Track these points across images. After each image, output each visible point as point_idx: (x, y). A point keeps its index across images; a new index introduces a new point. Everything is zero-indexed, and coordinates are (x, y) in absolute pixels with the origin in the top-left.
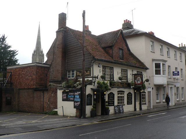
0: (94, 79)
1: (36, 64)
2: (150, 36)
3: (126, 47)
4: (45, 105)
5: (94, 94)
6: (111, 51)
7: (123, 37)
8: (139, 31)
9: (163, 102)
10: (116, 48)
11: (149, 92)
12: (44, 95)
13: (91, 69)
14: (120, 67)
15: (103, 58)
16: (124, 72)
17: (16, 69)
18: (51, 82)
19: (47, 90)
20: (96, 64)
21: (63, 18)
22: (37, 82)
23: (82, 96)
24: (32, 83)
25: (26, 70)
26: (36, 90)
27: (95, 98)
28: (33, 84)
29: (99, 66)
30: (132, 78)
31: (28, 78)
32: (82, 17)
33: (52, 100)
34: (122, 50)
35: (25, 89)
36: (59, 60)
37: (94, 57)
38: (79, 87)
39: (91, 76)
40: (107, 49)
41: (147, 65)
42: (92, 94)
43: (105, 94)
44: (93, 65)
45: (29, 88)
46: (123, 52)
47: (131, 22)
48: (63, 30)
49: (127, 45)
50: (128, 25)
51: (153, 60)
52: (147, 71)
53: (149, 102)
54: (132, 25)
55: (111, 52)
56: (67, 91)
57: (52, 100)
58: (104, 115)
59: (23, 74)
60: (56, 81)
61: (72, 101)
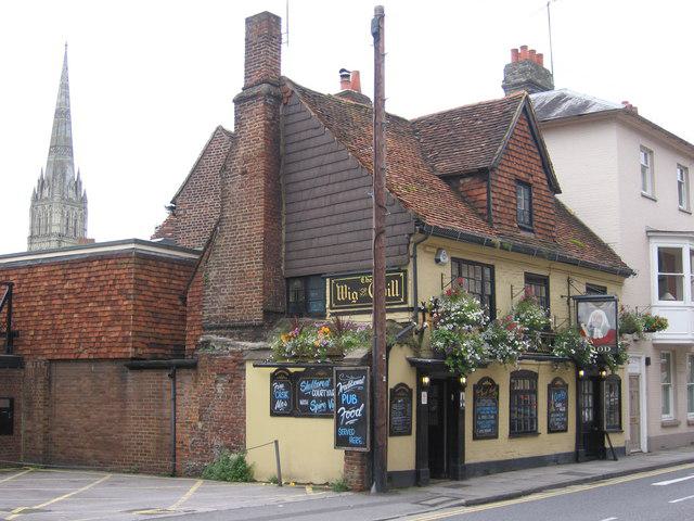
0: (420, 315)
1: (133, 246)
2: (627, 118)
3: (544, 177)
4: (184, 435)
5: (421, 386)
6: (485, 190)
7: (530, 125)
8: (586, 104)
9: (688, 422)
10: (503, 180)
11: (635, 378)
12: (175, 389)
13: (405, 272)
14: (517, 263)
15: (456, 226)
16: (537, 281)
17: (30, 267)
18: (210, 329)
19: (194, 366)
20: (428, 249)
21: (264, 33)
22: (142, 329)
23: (372, 395)
24: (115, 332)
25: (86, 275)
26: (136, 365)
27: (424, 401)
28: (120, 340)
29: (438, 261)
30: (566, 315)
31: (98, 310)
32: (372, 38)
33: (217, 410)
34: (528, 185)
35: (77, 360)
36: (249, 224)
37: (418, 222)
38: (359, 353)
39: (406, 302)
40: (462, 182)
41: (629, 260)
42: (412, 384)
43: (462, 387)
44: (415, 257)
45: (102, 356)
46: (530, 194)
47: (541, 56)
48: (269, 94)
49: (546, 166)
50: (528, 71)
51: (652, 233)
52: (628, 281)
53: (635, 422)
54: (547, 71)
55: (484, 197)
56: (292, 370)
57: (217, 410)
58: (457, 480)
59: (69, 291)
60: (240, 327)
61: (325, 414)
